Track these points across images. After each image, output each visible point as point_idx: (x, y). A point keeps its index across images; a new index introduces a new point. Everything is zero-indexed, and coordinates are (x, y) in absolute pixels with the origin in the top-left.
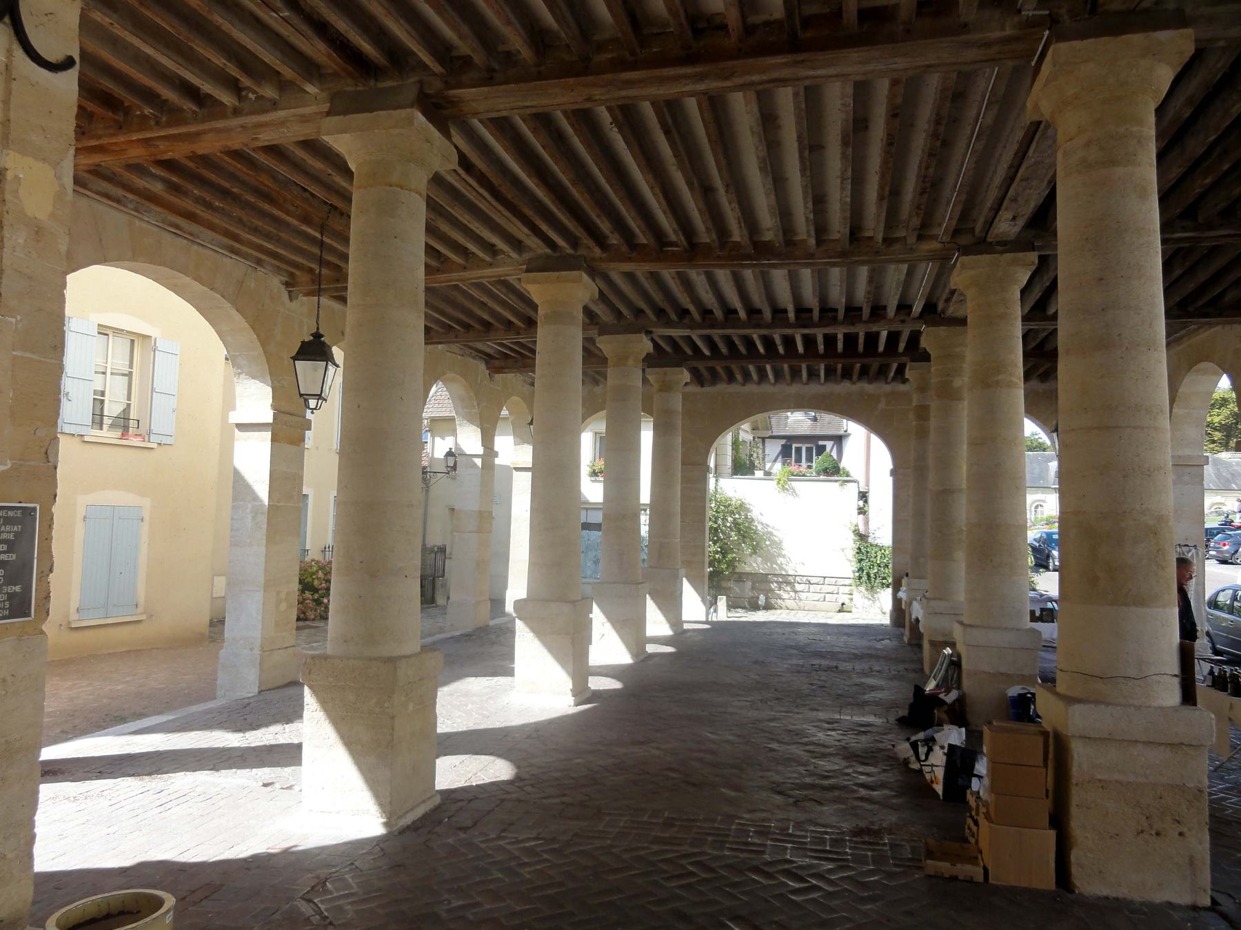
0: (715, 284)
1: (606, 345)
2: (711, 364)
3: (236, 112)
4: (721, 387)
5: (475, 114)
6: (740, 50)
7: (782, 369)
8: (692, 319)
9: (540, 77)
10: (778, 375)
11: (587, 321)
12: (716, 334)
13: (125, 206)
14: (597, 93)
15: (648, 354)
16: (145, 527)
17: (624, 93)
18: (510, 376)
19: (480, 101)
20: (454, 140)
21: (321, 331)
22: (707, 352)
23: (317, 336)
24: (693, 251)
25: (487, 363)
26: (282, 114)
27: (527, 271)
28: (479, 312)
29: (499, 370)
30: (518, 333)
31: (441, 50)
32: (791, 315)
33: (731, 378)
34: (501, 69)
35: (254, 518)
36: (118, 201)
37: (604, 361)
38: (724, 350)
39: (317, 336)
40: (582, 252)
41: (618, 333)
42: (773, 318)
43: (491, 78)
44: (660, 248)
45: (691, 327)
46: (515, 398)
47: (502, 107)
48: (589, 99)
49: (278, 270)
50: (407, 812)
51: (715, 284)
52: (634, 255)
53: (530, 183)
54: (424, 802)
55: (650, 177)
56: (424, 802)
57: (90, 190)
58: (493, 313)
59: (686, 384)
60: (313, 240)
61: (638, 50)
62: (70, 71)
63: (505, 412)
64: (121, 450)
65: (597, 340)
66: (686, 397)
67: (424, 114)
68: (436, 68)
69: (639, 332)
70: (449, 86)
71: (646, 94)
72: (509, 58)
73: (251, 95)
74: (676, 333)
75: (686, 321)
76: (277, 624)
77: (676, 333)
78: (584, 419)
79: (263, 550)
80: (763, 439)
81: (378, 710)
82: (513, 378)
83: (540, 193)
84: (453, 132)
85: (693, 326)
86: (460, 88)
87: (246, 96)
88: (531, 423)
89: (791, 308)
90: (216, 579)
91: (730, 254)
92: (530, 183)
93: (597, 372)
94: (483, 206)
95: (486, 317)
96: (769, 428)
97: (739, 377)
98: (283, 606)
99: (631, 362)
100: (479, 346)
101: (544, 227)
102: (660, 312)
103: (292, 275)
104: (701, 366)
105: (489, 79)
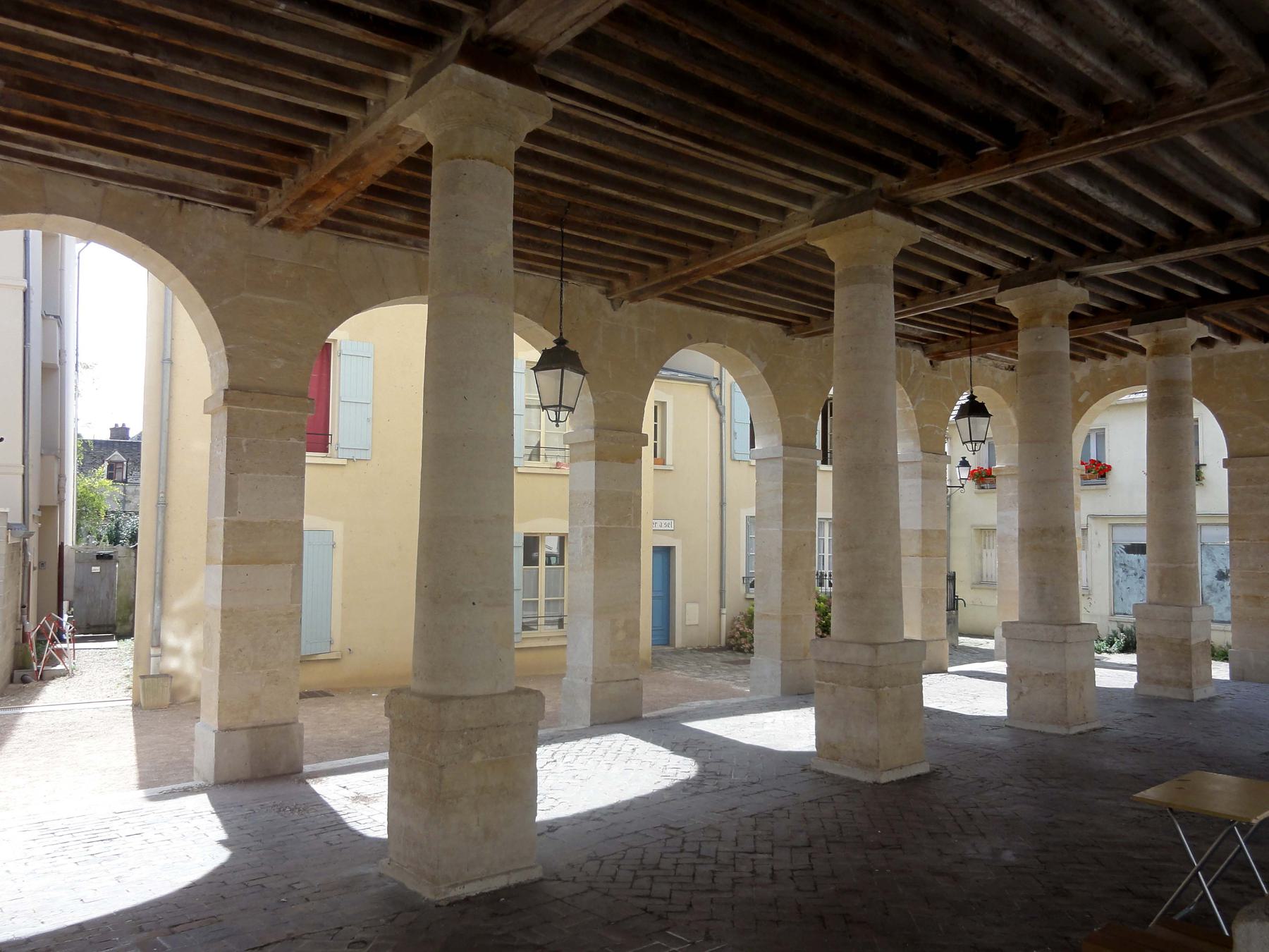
13: (404, 244)
16: (338, 557)
21: (564, 337)
25: (924, 349)
27: (814, 225)
29: (941, 356)
36: (395, 240)
40: (877, 185)
41: (1024, 284)
49: (592, 281)
50: (467, 882)
52: (940, 171)
54: (508, 873)
56: (508, 873)
57: (365, 235)
64: (554, 479)
65: (997, 297)
69: (1054, 276)
70: (489, 24)
79: (591, 575)
90: (689, 606)
99: (1046, 320)
103: (609, 283)
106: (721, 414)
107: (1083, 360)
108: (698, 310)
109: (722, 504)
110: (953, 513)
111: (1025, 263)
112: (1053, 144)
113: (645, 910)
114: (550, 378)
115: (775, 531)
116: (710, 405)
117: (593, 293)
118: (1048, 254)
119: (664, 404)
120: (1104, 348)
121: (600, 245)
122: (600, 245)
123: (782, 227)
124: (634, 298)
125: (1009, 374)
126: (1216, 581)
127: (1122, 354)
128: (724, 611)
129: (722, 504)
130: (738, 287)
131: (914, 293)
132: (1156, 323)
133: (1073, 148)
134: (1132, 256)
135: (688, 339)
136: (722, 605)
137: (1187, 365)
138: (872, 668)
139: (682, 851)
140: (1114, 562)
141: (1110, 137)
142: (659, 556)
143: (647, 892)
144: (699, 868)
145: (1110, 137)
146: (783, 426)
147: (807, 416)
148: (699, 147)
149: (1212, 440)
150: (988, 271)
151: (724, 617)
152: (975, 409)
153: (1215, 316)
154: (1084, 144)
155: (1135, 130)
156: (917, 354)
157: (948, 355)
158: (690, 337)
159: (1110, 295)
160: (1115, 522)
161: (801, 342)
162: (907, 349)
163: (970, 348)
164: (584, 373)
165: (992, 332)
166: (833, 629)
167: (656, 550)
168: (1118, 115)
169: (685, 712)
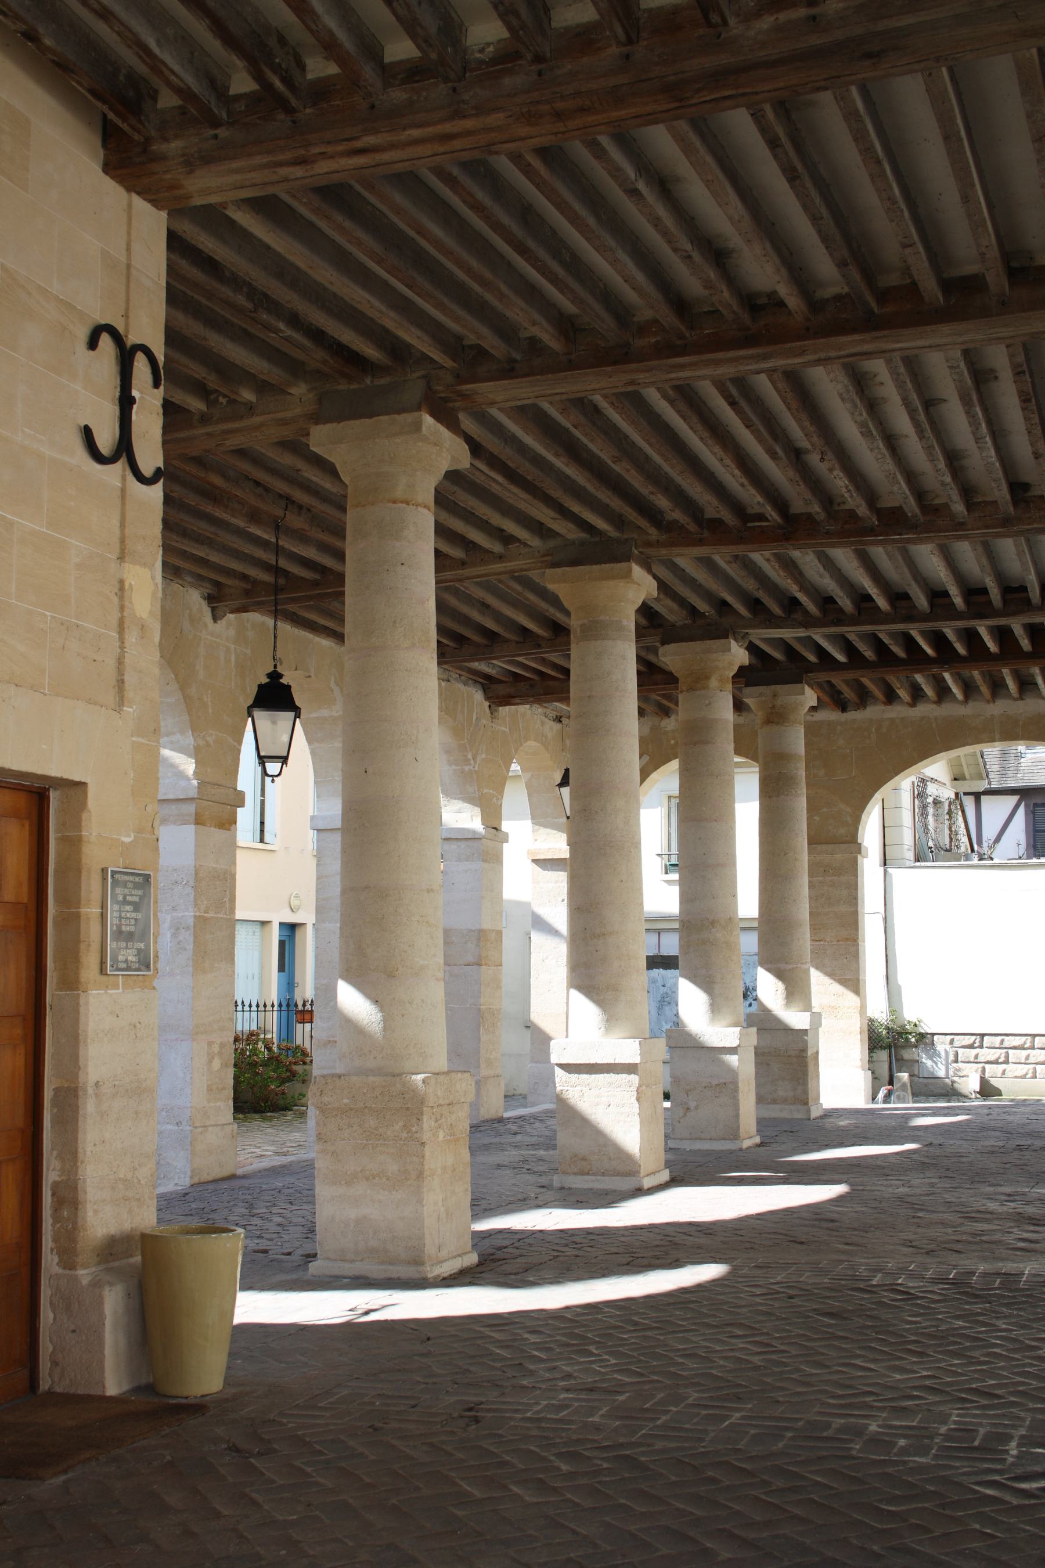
0: (832, 567)
1: (671, 657)
2: (851, 675)
3: (204, 419)
4: (875, 712)
5: (493, 403)
6: (808, 329)
7: (972, 677)
8: (806, 612)
9: (571, 366)
10: (969, 689)
11: (644, 622)
12: (852, 633)
14: (641, 377)
15: (741, 668)
17: (673, 375)
18: (523, 709)
19: (499, 397)
20: (463, 427)
22: (841, 658)
23: (275, 676)
24: (794, 528)
25: (485, 690)
26: (257, 419)
28: (476, 615)
29: (506, 700)
30: (539, 646)
31: (453, 345)
32: (958, 601)
33: (891, 697)
34: (528, 361)
35: (174, 935)
37: (671, 679)
38: (869, 654)
39: (275, 676)
42: (932, 605)
43: (513, 369)
44: (745, 528)
45: (806, 625)
46: (532, 744)
47: (524, 395)
48: (632, 383)
51: (832, 567)
53: (559, 463)
55: (717, 449)
58: (498, 617)
59: (813, 709)
60: (265, 544)
61: (688, 335)
62: (153, 486)
63: (515, 767)
66: (811, 730)
67: (432, 415)
68: (448, 363)
70: (460, 379)
71: (706, 379)
72: (534, 345)
73: (221, 399)
74: (787, 634)
75: (798, 616)
76: (210, 1089)
77: (787, 634)
78: (645, 774)
80: (977, 796)
81: (405, 1135)
82: (530, 716)
83: (572, 471)
84: (462, 416)
85: (809, 622)
86: (474, 382)
87: (216, 400)
88: (565, 782)
89: (954, 591)
91: (849, 528)
92: (559, 463)
93: (664, 696)
94: (495, 489)
95: (490, 624)
96: (983, 774)
97: (903, 694)
98: (217, 1064)
100: (475, 665)
101: (576, 508)
102: (755, 605)
104: (838, 680)
105: (509, 371)
112: (827, 533)
125: (557, 726)
157: (517, 700)
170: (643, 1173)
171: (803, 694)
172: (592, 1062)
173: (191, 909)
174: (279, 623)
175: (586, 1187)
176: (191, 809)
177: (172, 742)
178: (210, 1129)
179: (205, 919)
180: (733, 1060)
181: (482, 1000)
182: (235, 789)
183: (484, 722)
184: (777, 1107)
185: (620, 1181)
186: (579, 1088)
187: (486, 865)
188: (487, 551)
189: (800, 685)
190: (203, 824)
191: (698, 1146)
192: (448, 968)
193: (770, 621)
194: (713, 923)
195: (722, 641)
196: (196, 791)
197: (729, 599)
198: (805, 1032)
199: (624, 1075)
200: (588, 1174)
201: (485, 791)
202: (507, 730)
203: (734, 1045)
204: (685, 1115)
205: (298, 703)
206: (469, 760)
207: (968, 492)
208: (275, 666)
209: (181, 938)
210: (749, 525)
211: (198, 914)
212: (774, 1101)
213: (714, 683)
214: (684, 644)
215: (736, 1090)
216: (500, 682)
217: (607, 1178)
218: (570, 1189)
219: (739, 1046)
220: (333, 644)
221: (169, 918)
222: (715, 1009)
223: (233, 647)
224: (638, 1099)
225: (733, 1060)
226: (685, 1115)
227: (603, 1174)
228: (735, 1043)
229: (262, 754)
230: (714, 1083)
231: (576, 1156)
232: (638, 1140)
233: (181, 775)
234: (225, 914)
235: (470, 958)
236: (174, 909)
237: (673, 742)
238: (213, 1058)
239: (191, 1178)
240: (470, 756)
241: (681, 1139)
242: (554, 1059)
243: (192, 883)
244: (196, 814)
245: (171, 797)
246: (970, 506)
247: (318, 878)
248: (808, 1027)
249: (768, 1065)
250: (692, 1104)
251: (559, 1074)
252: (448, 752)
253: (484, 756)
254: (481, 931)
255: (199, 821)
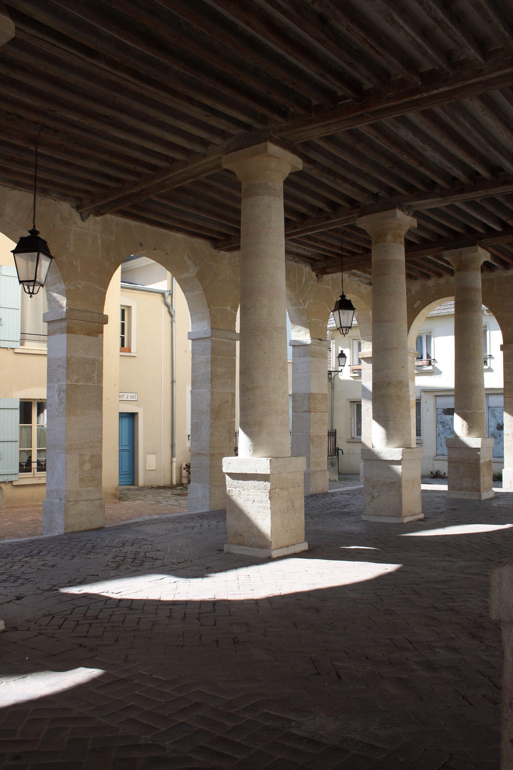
23: (34, 232)
90: (148, 456)
103: (80, 199)
106: (172, 316)
107: (416, 278)
108: (148, 226)
109: (173, 382)
110: (335, 389)
111: (376, 196)
112: (388, 98)
113: (81, 645)
114: (21, 258)
115: (205, 391)
116: (164, 309)
117: (66, 207)
118: (391, 191)
119: (129, 307)
120: (429, 270)
121: (69, 164)
122: (69, 164)
123: (204, 156)
124: (98, 213)
125: (369, 288)
126: (496, 431)
127: (440, 275)
128: (174, 459)
129: (173, 382)
130: (175, 206)
131: (304, 216)
132: (459, 249)
133: (401, 101)
134: (443, 195)
135: (140, 248)
136: (173, 455)
137: (477, 279)
138: (41, 130)
139: (118, 607)
140: (437, 420)
141: (425, 95)
142: (126, 422)
143: (84, 634)
144: (127, 616)
145: (425, 95)
146: (211, 315)
147: (229, 308)
148: (138, 82)
149: (495, 338)
150: (353, 202)
151: (174, 464)
152: (344, 304)
153: (493, 246)
154: (407, 100)
155: (441, 90)
156: (307, 269)
157: (328, 270)
158: (141, 245)
159: (431, 227)
160: (437, 393)
161: (226, 256)
162: (300, 265)
163: (342, 265)
164: (51, 257)
165: (357, 254)
166: (240, 451)
167: (122, 415)
168: (431, 78)
169: (137, 523)
170: (273, 546)
171: (477, 252)
172: (244, 472)
173: (65, 381)
174: (38, 198)
175: (241, 553)
176: (64, 324)
177: (57, 289)
178: (82, 502)
179: (76, 386)
180: (399, 468)
181: (311, 431)
182: (102, 314)
183: (312, 283)
184: (462, 492)
185: (254, 551)
186: (238, 489)
187: (314, 359)
188: (198, 153)
189: (474, 247)
190: (75, 333)
191: (378, 519)
192: (294, 414)
193: (420, 195)
194: (389, 384)
195: (392, 211)
196: (65, 314)
197: (392, 185)
198: (478, 449)
199: (262, 482)
200: (243, 545)
201: (313, 320)
202: (330, 288)
203: (399, 459)
204: (372, 501)
205: (354, 307)
206: (301, 303)
207: (481, 44)
208: (34, 226)
209: (61, 397)
210: (339, 103)
211: (70, 383)
212: (461, 489)
213: (389, 238)
214: (370, 215)
215: (400, 487)
216: (319, 261)
217: (252, 549)
218: (232, 554)
219: (402, 459)
220: (186, 237)
221: (56, 385)
222: (389, 437)
223: (99, 235)
224: (270, 498)
225: (399, 468)
226: (372, 501)
227: (251, 546)
228: (399, 458)
229: (21, 280)
230: (388, 482)
231: (236, 532)
232: (270, 525)
233: (61, 307)
234: (94, 383)
235: (305, 409)
236: (59, 381)
237: (432, 292)
238: (84, 463)
239: (65, 529)
240: (301, 301)
241: (369, 515)
242: (224, 470)
243: (65, 366)
244: (67, 327)
245: (56, 319)
246: (485, 55)
247: (192, 366)
248: (480, 447)
249: (458, 468)
250: (376, 494)
251: (228, 478)
252: (290, 299)
253: (311, 301)
254: (310, 394)
255: (69, 331)
